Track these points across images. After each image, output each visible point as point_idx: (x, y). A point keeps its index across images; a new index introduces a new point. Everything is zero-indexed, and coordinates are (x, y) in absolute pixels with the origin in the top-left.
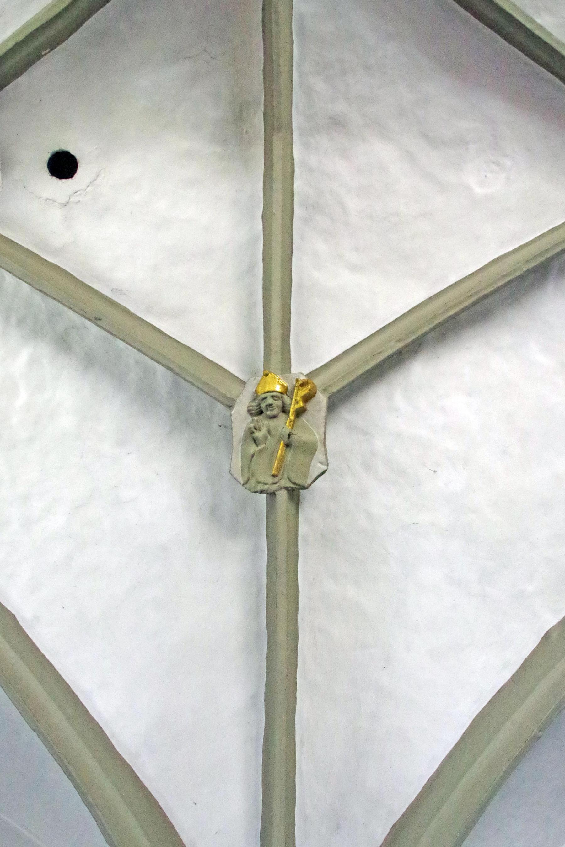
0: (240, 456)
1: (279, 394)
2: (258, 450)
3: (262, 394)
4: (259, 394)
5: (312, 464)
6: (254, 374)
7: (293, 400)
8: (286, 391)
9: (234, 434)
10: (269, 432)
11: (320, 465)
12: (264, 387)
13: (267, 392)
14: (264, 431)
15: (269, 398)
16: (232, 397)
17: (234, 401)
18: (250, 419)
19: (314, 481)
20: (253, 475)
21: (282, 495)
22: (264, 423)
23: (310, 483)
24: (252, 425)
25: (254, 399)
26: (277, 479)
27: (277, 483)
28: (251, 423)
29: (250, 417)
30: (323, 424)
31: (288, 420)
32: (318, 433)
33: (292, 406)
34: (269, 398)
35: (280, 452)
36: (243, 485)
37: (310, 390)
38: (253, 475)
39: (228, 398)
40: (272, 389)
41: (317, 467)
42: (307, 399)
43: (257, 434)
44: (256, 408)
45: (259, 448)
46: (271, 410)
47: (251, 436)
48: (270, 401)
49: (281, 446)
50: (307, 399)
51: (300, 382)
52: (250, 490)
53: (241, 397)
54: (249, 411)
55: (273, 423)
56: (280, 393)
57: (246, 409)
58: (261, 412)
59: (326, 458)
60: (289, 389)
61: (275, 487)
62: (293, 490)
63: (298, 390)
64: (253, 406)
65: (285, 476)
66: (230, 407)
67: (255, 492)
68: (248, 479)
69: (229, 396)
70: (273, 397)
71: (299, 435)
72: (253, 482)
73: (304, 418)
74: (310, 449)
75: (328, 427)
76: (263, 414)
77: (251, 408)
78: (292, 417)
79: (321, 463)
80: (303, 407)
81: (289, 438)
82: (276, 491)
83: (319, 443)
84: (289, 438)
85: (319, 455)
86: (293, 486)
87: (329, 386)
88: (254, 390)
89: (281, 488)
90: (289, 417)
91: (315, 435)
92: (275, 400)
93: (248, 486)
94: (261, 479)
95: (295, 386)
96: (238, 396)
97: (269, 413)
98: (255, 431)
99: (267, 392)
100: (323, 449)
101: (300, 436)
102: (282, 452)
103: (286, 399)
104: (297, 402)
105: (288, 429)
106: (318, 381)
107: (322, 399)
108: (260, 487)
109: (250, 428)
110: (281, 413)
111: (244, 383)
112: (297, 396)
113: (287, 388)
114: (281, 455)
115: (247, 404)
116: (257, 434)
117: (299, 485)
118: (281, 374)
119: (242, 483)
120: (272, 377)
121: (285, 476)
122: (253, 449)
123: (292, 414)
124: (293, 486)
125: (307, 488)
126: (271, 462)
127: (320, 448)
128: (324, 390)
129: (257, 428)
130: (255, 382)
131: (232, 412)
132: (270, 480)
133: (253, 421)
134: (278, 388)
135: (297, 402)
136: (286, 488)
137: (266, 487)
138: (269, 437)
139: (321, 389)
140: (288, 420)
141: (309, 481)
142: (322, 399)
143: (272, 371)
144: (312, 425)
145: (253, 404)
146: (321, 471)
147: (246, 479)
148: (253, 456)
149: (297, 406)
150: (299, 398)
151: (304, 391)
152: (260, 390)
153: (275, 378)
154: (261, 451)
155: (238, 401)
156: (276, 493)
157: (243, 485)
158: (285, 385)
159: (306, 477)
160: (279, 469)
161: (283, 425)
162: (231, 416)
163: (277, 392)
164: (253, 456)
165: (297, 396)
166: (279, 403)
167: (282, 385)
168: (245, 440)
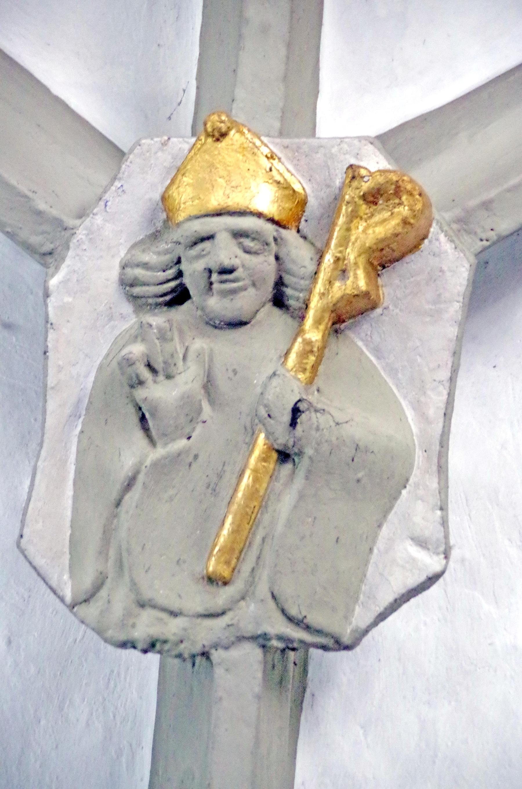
0: (71, 476)
1: (270, 228)
2: (155, 464)
3: (191, 218)
4: (181, 216)
5: (380, 544)
6: (151, 115)
7: (328, 259)
8: (293, 215)
9: (51, 381)
10: (209, 385)
11: (415, 551)
12: (202, 187)
13: (219, 214)
14: (188, 379)
15: (223, 239)
16: (55, 212)
17: (63, 230)
18: (128, 318)
19: (382, 617)
20: (120, 565)
21: (241, 670)
22: (195, 349)
23: (363, 625)
24: (137, 349)
25: (155, 236)
26: (223, 596)
27: (223, 613)
28: (135, 339)
29: (127, 308)
30: (445, 374)
31: (298, 346)
32: (418, 407)
33: (319, 287)
34: (223, 239)
35: (247, 480)
36: (72, 607)
37: (405, 222)
38: (120, 565)
39: (39, 213)
40: (237, 200)
41: (400, 559)
42: (383, 259)
43: (159, 393)
44: (161, 276)
45: (160, 452)
46: (225, 294)
47: (128, 397)
48: (226, 252)
49: (257, 453)
50: (383, 259)
51: (365, 186)
52: (100, 632)
53: (99, 220)
54: (128, 284)
55: (226, 348)
56: (272, 220)
57: (115, 273)
58: (180, 296)
59: (444, 522)
60: (312, 202)
61: (206, 632)
62: (289, 646)
63: (354, 216)
64: (146, 266)
65: (263, 589)
66: (48, 258)
67: (127, 644)
68: (98, 587)
69: (42, 206)
70: (238, 235)
71: (339, 417)
72: (117, 599)
73: (359, 340)
74: (374, 479)
75: (461, 382)
76: (187, 305)
77: (139, 272)
78: (314, 334)
79: (422, 543)
80: (367, 294)
81: (293, 423)
82: (216, 646)
83: (419, 457)
84: (293, 423)
85: (414, 508)
86: (297, 634)
87: (486, 205)
88: (157, 196)
89: (241, 639)
90: (300, 332)
91: (403, 418)
92: (247, 251)
93: (91, 611)
94: (163, 595)
95: (337, 199)
96: (82, 214)
97: (214, 303)
98: (146, 374)
99: (219, 214)
100: (434, 484)
101: (346, 414)
102: (256, 480)
103: (298, 251)
104: (342, 271)
105: (289, 388)
106: (434, 176)
107: (448, 262)
108: (145, 625)
109: (129, 362)
110: (269, 306)
111: (119, 155)
112: (344, 242)
113: (303, 203)
114: (252, 494)
115: (123, 253)
116: (159, 393)
117: (319, 632)
118: (281, 134)
119: (68, 597)
120: (243, 148)
121: (263, 589)
122: (132, 452)
123: (318, 322)
124: (297, 634)
125: (347, 648)
126: (206, 521)
127: (422, 475)
128: (464, 224)
129: (159, 365)
130: (165, 159)
131: (53, 282)
132: (197, 599)
133: (141, 334)
134: (265, 199)
135: (342, 271)
136: (262, 640)
137: (173, 627)
138: (206, 407)
139: (448, 216)
140: (298, 346)
141: (361, 617)
142: (448, 262)
143: (241, 118)
144: (393, 371)
145: (146, 258)
146: (413, 581)
147: (87, 581)
148: (130, 484)
149: (339, 289)
150: (351, 254)
151: (379, 227)
152: (187, 199)
153: (254, 152)
154: (161, 468)
155: (81, 234)
156: (216, 655)
157: (72, 607)
158: (298, 188)
159: (353, 597)
160: (236, 551)
161: (270, 361)
162: (47, 295)
163: (260, 215)
164: (130, 484)
165: (344, 242)
166: (265, 265)
167: (284, 187)
168: (97, 408)
